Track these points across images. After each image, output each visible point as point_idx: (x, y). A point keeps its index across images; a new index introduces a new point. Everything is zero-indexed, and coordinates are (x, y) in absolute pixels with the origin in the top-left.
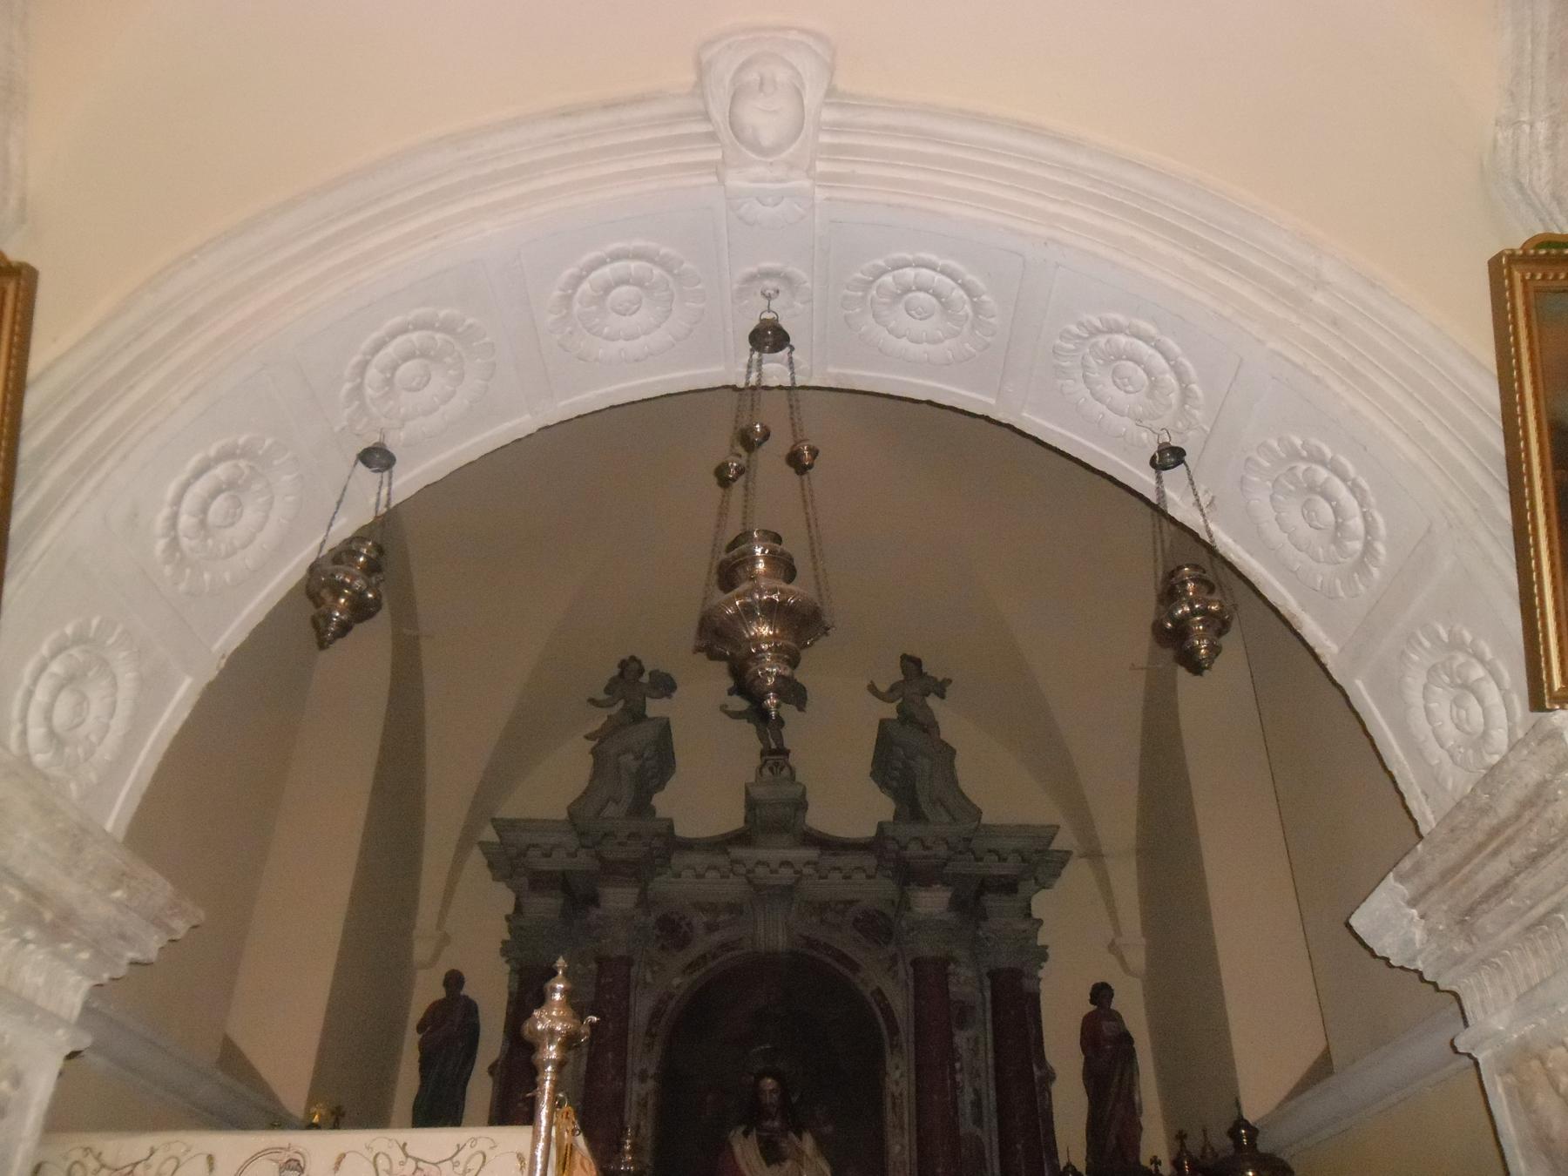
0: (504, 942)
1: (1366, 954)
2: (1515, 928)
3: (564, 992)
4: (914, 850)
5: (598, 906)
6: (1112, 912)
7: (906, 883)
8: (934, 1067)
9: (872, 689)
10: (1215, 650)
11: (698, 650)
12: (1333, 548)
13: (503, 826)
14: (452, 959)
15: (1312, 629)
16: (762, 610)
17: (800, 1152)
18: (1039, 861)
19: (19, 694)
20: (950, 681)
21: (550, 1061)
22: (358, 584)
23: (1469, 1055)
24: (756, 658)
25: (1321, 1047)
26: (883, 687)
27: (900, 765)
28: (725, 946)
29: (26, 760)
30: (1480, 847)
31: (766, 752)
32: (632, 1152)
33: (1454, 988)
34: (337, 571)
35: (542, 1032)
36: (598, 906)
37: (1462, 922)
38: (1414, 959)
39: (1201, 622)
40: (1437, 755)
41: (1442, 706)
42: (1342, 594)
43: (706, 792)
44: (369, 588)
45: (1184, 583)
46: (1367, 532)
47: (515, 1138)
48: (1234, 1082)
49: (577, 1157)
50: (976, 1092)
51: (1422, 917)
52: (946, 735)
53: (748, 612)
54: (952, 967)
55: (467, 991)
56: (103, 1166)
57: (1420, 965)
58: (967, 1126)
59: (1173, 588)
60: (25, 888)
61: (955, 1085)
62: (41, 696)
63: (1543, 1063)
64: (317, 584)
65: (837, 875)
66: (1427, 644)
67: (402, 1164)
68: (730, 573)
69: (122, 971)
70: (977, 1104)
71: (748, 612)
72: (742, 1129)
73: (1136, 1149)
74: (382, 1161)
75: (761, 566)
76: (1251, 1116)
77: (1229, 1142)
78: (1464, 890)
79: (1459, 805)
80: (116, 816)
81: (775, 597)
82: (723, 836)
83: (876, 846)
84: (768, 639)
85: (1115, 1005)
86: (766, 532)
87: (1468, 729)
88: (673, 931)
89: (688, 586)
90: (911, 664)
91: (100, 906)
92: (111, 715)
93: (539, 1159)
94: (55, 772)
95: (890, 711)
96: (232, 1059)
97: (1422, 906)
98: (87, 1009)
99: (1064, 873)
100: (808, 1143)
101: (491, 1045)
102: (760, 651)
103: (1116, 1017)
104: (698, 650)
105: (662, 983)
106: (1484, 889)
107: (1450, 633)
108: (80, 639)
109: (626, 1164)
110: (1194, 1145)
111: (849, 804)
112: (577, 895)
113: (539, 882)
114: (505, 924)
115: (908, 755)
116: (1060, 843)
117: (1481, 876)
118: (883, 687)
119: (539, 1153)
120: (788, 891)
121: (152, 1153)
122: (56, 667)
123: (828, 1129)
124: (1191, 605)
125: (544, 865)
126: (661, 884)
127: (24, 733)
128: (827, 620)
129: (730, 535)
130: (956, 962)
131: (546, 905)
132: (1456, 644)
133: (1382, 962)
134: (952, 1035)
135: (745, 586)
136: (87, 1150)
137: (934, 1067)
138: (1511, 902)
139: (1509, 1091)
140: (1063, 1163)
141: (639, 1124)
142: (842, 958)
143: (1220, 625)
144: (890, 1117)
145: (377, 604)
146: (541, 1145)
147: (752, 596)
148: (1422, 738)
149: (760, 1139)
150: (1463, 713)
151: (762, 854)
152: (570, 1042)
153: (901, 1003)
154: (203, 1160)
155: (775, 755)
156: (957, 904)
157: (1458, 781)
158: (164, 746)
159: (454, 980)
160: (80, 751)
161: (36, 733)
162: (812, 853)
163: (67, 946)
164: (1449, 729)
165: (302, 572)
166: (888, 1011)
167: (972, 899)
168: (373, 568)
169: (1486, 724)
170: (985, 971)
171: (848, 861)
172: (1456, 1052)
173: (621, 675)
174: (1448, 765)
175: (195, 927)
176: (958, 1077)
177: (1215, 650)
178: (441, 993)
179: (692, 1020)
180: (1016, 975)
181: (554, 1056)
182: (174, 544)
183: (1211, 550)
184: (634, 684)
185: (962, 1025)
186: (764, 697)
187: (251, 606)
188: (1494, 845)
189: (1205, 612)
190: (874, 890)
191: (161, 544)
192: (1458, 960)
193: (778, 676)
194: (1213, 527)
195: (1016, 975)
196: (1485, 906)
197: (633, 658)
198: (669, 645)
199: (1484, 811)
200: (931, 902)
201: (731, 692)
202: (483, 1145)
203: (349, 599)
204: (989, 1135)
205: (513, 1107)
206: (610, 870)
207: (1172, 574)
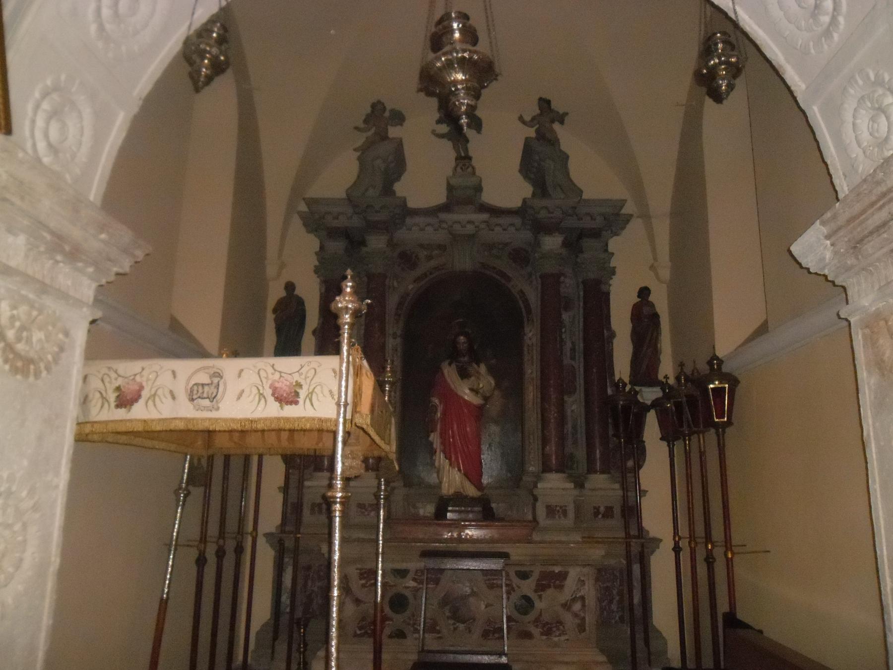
0: (315, 266)
1: (798, 266)
2: (885, 250)
3: (352, 287)
4: (543, 214)
5: (366, 246)
6: (654, 250)
7: (539, 233)
8: (551, 330)
9: (521, 119)
10: (731, 87)
11: (420, 90)
12: (811, 21)
13: (310, 202)
14: (286, 277)
15: (792, 76)
16: (458, 64)
17: (478, 372)
18: (614, 219)
19: (27, 123)
20: (567, 114)
21: (346, 323)
22: (215, 51)
23: (847, 320)
24: (455, 94)
25: (764, 317)
26: (527, 118)
27: (536, 165)
28: (436, 268)
29: (39, 160)
30: (873, 204)
31: (459, 158)
32: (391, 371)
33: (844, 284)
34: (201, 43)
35: (341, 308)
36: (366, 246)
37: (855, 247)
38: (824, 268)
39: (724, 69)
40: (856, 152)
41: (863, 123)
42: (813, 51)
43: (424, 181)
44: (221, 53)
45: (716, 44)
46: (835, 9)
47: (329, 362)
48: (713, 340)
49: (364, 371)
50: (573, 343)
51: (832, 245)
52: (564, 147)
53: (449, 65)
54: (562, 278)
55: (297, 292)
56: (119, 376)
57: (826, 272)
58: (567, 361)
59: (710, 47)
60: (52, 233)
61: (562, 340)
62: (40, 123)
63: (887, 322)
64: (190, 52)
65: (497, 229)
66: (860, 82)
67: (273, 374)
68: (438, 40)
69: (112, 278)
70: (573, 350)
71: (449, 65)
72: (447, 363)
73: (657, 372)
74: (263, 374)
75: (457, 35)
76: (720, 353)
77: (707, 367)
78: (859, 229)
79: (865, 181)
80: (95, 192)
81: (466, 55)
82: (436, 206)
83: (521, 212)
84: (462, 82)
85: (651, 298)
86: (460, 13)
87: (876, 135)
88: (407, 260)
89: (413, 51)
90: (545, 104)
91: (95, 242)
92: (82, 135)
93: (344, 372)
94: (56, 168)
95: (531, 132)
96: (175, 326)
97: (833, 239)
98: (97, 300)
99: (628, 226)
100: (483, 369)
101: (313, 320)
102: (457, 89)
103: (652, 305)
104: (420, 90)
105: (405, 286)
106: (871, 228)
107: (876, 75)
108: (56, 88)
109: (389, 377)
110: (688, 370)
111: (506, 188)
112: (354, 240)
113: (333, 233)
114: (315, 257)
115: (541, 159)
116: (628, 209)
117: (870, 222)
118: (527, 118)
119: (344, 369)
120: (471, 237)
121: (143, 369)
122: (46, 106)
123: (493, 361)
124: (719, 59)
125: (335, 223)
126: (401, 234)
127: (34, 145)
128: (497, 70)
129: (437, 17)
130: (566, 277)
131: (337, 246)
132: (879, 82)
133: (806, 271)
134: (561, 315)
135: (446, 49)
136: (109, 368)
137: (551, 330)
138: (885, 235)
139: (865, 337)
140: (617, 378)
141: (393, 343)
142: (504, 275)
143: (735, 71)
144: (526, 358)
145: (227, 63)
146: (344, 365)
147: (452, 55)
148: (848, 142)
149: (457, 366)
150: (876, 125)
151: (455, 217)
152: (356, 314)
153: (534, 298)
154: (170, 373)
155: (464, 160)
156: (566, 244)
157: (865, 167)
158: (114, 153)
159: (290, 287)
160: (68, 155)
161: (41, 146)
162: (485, 216)
163: (80, 264)
164: (865, 136)
165: (179, 46)
166: (526, 302)
167: (575, 241)
168: (222, 40)
169: (888, 132)
170: (580, 280)
171: (504, 220)
172: (840, 318)
173: (373, 112)
174: (861, 157)
175: (147, 255)
176: (564, 336)
177: (731, 87)
178: (283, 294)
179: (420, 308)
180: (598, 282)
181: (348, 320)
182: (101, 28)
183: (735, 25)
184: (381, 118)
185: (567, 308)
186: (459, 118)
187: (152, 67)
188: (881, 203)
189: (727, 63)
190: (521, 237)
191: (93, 28)
192: (848, 269)
193: (468, 105)
194: (738, 8)
195: (598, 282)
196: (870, 238)
197: (379, 102)
198: (402, 92)
199: (878, 183)
200: (552, 243)
201: (439, 122)
202: (314, 365)
203: (209, 60)
204: (579, 366)
205: (328, 344)
206: (373, 227)
207: (709, 39)
